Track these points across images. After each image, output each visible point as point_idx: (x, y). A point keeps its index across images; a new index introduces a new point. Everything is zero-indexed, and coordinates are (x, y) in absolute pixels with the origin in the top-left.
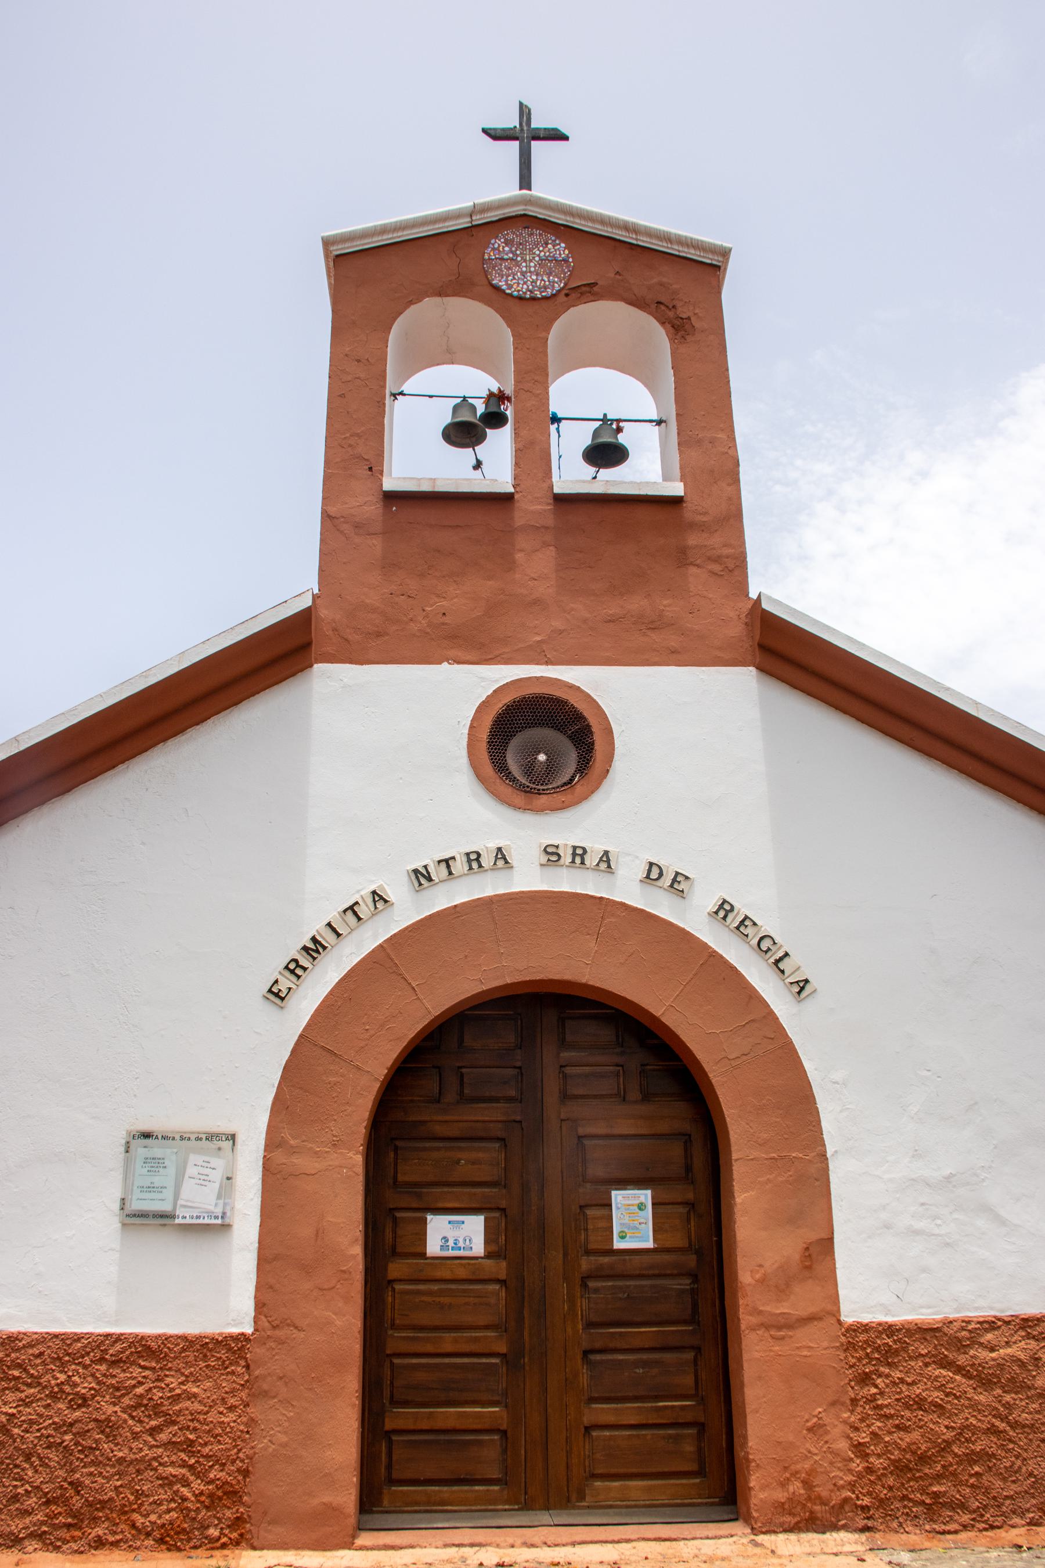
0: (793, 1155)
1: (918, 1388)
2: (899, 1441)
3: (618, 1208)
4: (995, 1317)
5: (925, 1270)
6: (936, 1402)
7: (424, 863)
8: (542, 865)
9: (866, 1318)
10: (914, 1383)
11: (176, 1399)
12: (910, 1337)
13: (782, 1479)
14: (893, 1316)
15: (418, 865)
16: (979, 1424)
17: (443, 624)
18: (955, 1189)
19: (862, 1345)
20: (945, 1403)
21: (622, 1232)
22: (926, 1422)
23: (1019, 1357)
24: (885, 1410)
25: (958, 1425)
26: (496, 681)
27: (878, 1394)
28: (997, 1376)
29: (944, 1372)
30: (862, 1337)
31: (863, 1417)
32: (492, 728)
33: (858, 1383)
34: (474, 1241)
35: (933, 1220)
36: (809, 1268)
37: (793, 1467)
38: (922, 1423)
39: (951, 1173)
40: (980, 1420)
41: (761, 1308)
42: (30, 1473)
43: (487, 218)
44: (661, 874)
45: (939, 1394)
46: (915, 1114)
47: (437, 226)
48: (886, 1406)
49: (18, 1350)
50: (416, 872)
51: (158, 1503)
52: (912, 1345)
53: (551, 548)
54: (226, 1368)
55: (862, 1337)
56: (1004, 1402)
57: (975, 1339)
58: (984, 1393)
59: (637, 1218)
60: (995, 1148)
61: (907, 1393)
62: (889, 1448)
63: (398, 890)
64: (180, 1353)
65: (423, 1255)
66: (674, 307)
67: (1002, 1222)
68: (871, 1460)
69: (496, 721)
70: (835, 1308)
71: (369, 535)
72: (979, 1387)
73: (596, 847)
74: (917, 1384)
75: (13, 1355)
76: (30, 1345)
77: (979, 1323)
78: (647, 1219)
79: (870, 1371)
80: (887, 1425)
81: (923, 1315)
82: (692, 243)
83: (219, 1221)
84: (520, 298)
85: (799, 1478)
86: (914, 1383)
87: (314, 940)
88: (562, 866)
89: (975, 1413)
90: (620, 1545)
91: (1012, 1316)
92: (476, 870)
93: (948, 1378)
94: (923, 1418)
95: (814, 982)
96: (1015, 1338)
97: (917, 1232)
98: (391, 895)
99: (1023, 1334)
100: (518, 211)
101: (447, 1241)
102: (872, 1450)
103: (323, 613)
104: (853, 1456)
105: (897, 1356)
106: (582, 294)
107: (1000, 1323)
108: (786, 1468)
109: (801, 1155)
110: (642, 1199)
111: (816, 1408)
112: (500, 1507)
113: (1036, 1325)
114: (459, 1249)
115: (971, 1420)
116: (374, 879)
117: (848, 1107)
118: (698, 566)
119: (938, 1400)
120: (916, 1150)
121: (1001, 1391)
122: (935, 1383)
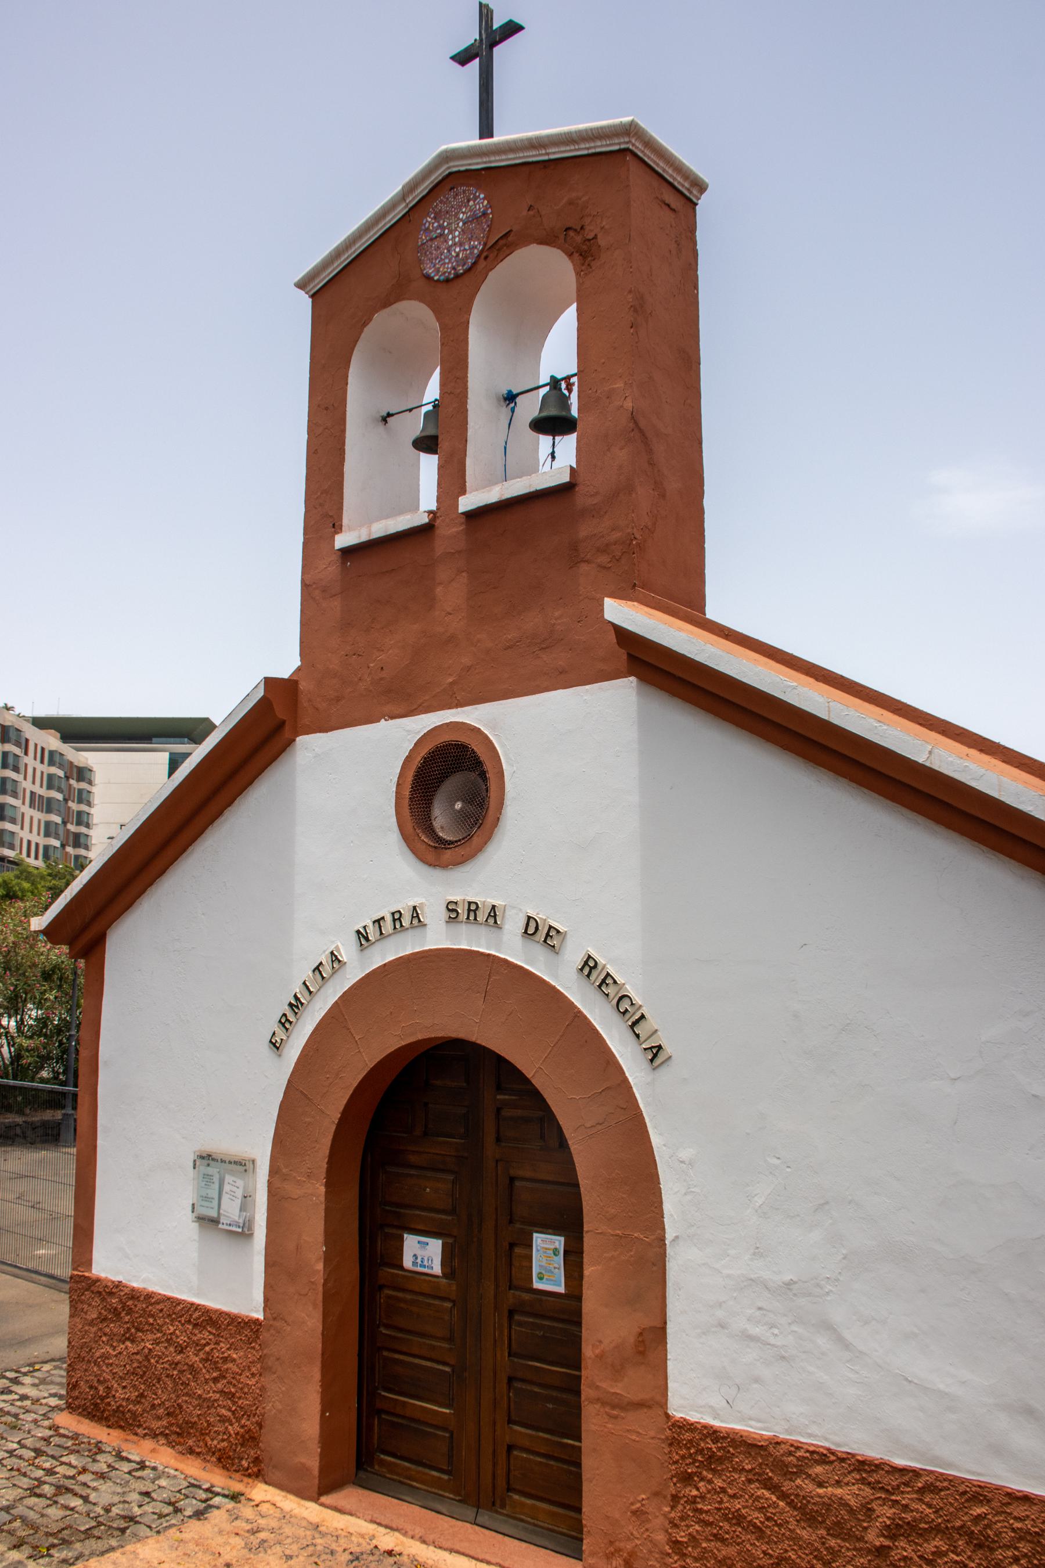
0: (635, 1235)
1: (739, 1503)
2: (715, 1551)
3: (538, 1250)
4: (829, 1449)
5: (757, 1380)
6: (755, 1523)
7: (364, 924)
8: (447, 922)
9: (693, 1417)
10: (734, 1496)
11: (225, 1360)
12: (735, 1448)
13: (607, 1552)
14: (722, 1421)
15: (359, 927)
16: (798, 1561)
17: (381, 679)
18: (795, 1298)
19: (686, 1444)
20: (765, 1527)
21: (541, 1273)
22: (744, 1541)
23: (848, 1502)
24: (704, 1515)
25: (776, 1554)
26: (419, 732)
27: (699, 1497)
28: (822, 1515)
29: (767, 1494)
30: (687, 1436)
31: (682, 1515)
32: (414, 784)
33: (680, 1480)
34: (434, 1262)
35: (770, 1328)
36: (642, 1353)
37: (617, 1543)
38: (739, 1540)
39: (791, 1280)
40: (800, 1557)
41: (598, 1384)
42: (160, 1392)
43: (418, 194)
44: (537, 928)
45: (759, 1516)
46: (760, 1207)
47: (380, 226)
48: (707, 1512)
49: (152, 1304)
50: (358, 932)
51: (217, 1433)
52: (737, 1457)
53: (464, 574)
54: (251, 1343)
55: (687, 1436)
56: (827, 1545)
57: (802, 1468)
58: (808, 1529)
59: (552, 1262)
60: (844, 1258)
61: (727, 1504)
62: (706, 1555)
63: (348, 952)
64: (228, 1326)
65: (401, 1267)
66: (582, 228)
67: (847, 1346)
68: (688, 1560)
69: (416, 776)
70: (664, 1401)
71: (331, 597)
72: (803, 1520)
73: (485, 899)
74: (738, 1498)
75: (150, 1308)
76: (157, 1303)
77: (808, 1451)
78: (560, 1265)
79: (692, 1472)
80: (705, 1531)
81: (751, 1427)
82: (593, 135)
83: (240, 1230)
84: (447, 281)
85: (622, 1556)
86: (734, 1496)
87: (296, 997)
88: (462, 922)
89: (795, 1548)
90: (482, 1564)
91: (848, 1453)
92: (399, 929)
93: (771, 1502)
94: (741, 1536)
95: (669, 1049)
96: (848, 1479)
97: (752, 1338)
98: (344, 957)
99: (858, 1477)
100: (443, 172)
101: (417, 1258)
102: (689, 1552)
103: (303, 686)
104: (670, 1551)
105: (721, 1463)
106: (499, 250)
107: (832, 1458)
108: (611, 1543)
109: (642, 1236)
110: (557, 1244)
111: (640, 1494)
112: (447, 1494)
113: (873, 1470)
114: (424, 1266)
115: (790, 1554)
116: (334, 939)
117: (693, 1190)
118: (588, 562)
119: (757, 1521)
120: (758, 1248)
121: (826, 1533)
122: (756, 1503)
